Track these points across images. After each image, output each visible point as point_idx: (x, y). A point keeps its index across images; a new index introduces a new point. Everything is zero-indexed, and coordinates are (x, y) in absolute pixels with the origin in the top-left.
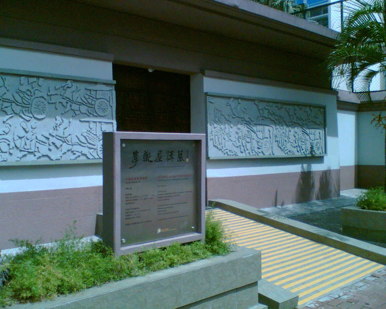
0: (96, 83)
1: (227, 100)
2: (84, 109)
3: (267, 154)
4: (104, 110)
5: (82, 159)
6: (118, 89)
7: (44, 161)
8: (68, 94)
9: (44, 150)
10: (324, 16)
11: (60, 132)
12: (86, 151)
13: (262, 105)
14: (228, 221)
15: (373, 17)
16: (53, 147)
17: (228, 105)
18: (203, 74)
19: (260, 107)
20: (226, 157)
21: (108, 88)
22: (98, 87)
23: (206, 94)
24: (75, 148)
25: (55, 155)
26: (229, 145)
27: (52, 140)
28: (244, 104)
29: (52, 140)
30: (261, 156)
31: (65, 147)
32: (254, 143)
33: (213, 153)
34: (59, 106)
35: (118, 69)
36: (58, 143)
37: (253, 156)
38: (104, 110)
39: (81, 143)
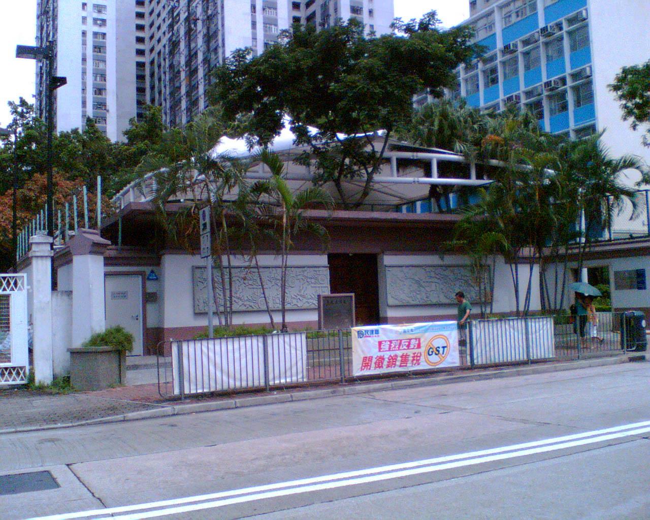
0: (319, 267)
1: (400, 269)
2: (313, 281)
3: (434, 301)
4: (323, 280)
5: (250, 309)
6: (330, 269)
7: (295, 307)
8: (305, 274)
9: (295, 302)
10: (453, 200)
11: (302, 293)
12: (252, 304)
13: (428, 269)
14: (512, 330)
15: (620, 241)
16: (298, 300)
17: (402, 271)
18: (384, 254)
19: (427, 270)
20: (401, 304)
21: (325, 269)
22: (320, 269)
23: (386, 266)
24: (309, 301)
25: (299, 305)
26: (403, 296)
27: (298, 297)
28: (414, 270)
29: (298, 297)
30: (429, 302)
31: (305, 300)
32: (424, 294)
33: (391, 301)
34: (302, 281)
35: (332, 258)
36: (237, 300)
37: (421, 303)
38: (323, 280)
39: (249, 300)
